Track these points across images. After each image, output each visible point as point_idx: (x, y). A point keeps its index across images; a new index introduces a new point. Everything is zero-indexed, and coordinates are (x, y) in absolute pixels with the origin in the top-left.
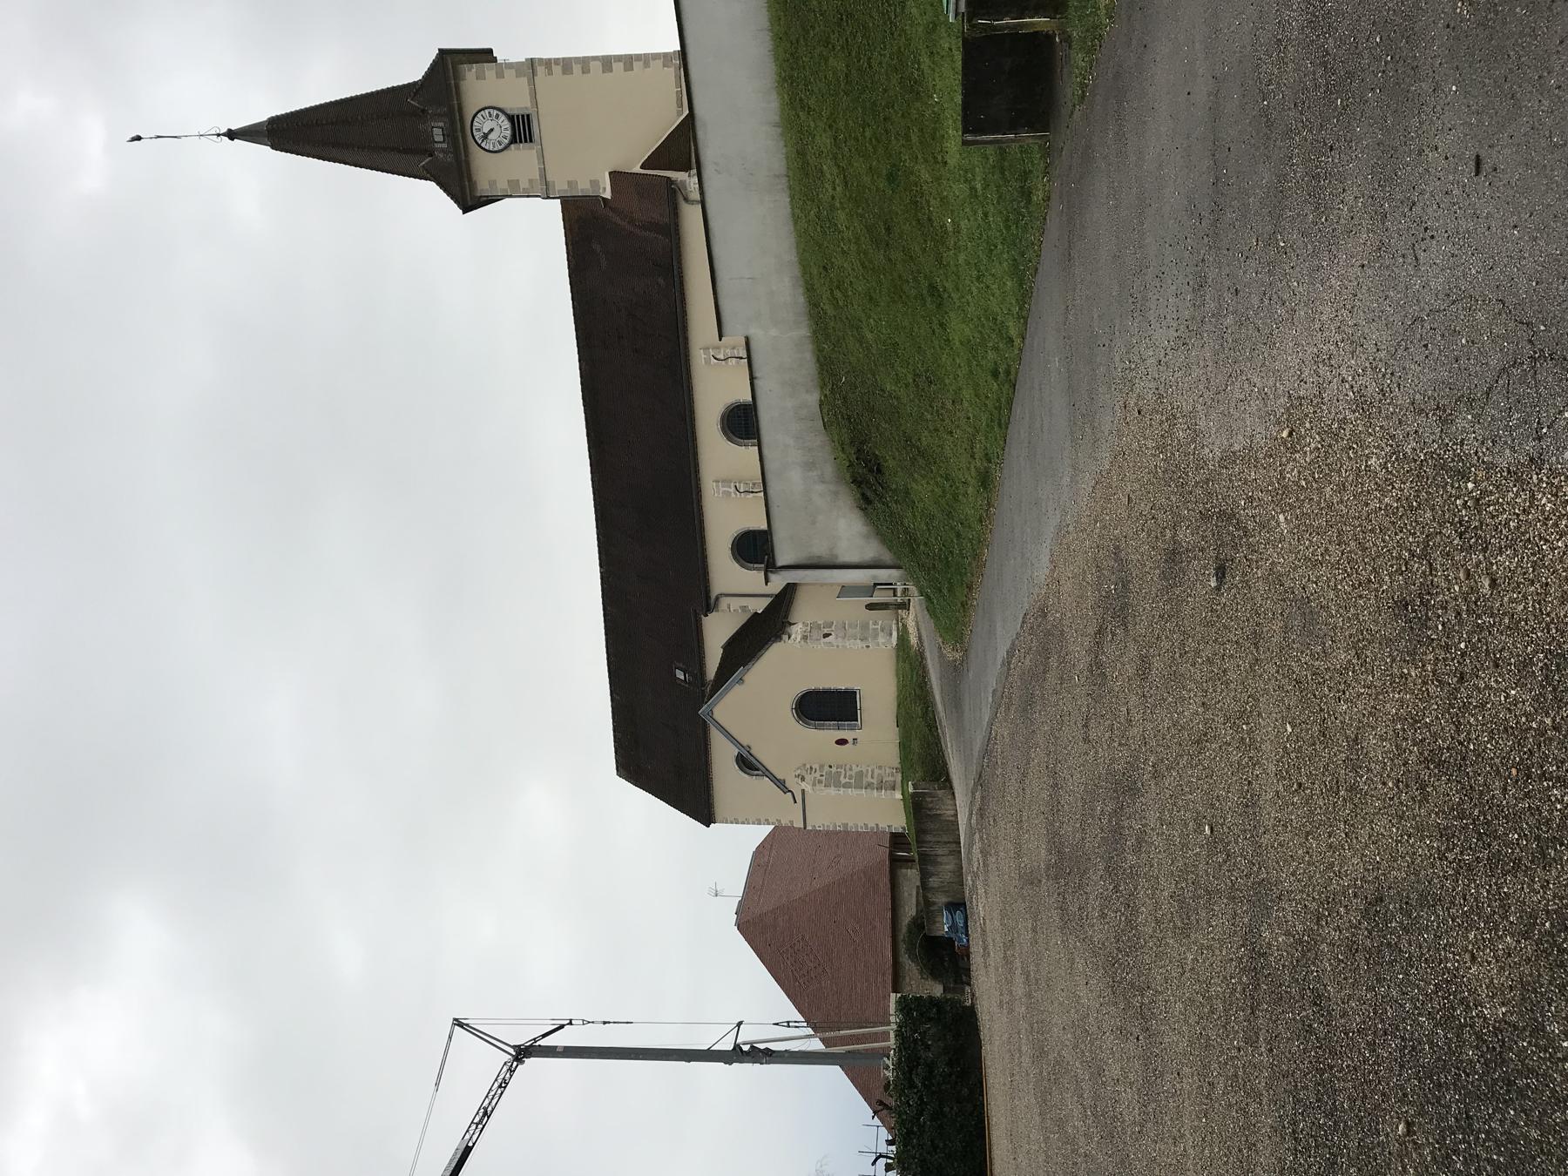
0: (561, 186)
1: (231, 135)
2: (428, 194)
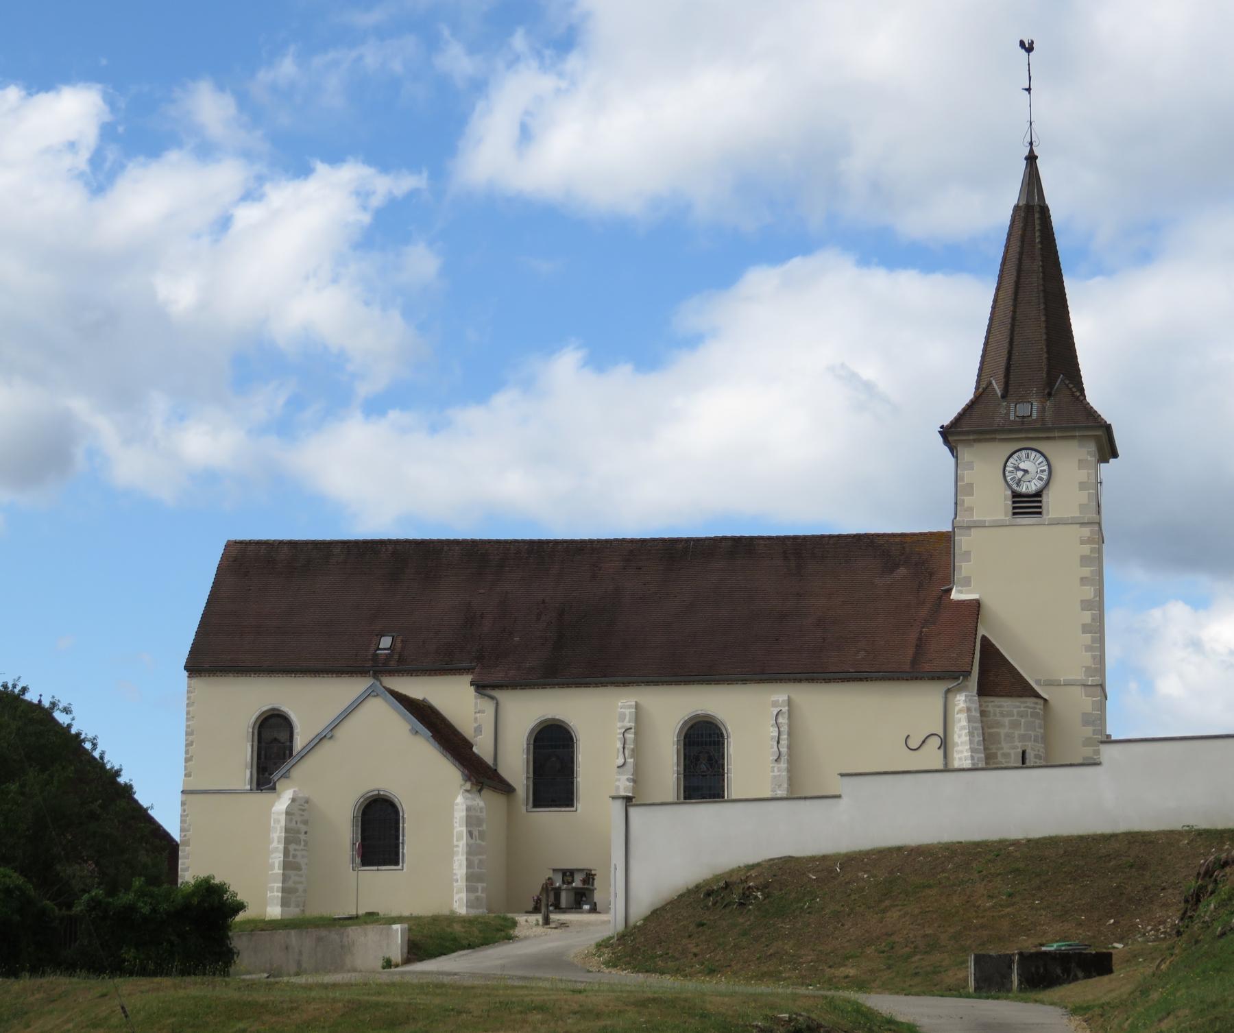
0: (963, 542)
1: (1031, 159)
2: (959, 389)
